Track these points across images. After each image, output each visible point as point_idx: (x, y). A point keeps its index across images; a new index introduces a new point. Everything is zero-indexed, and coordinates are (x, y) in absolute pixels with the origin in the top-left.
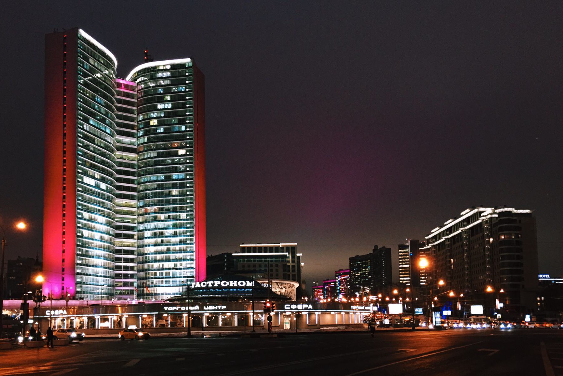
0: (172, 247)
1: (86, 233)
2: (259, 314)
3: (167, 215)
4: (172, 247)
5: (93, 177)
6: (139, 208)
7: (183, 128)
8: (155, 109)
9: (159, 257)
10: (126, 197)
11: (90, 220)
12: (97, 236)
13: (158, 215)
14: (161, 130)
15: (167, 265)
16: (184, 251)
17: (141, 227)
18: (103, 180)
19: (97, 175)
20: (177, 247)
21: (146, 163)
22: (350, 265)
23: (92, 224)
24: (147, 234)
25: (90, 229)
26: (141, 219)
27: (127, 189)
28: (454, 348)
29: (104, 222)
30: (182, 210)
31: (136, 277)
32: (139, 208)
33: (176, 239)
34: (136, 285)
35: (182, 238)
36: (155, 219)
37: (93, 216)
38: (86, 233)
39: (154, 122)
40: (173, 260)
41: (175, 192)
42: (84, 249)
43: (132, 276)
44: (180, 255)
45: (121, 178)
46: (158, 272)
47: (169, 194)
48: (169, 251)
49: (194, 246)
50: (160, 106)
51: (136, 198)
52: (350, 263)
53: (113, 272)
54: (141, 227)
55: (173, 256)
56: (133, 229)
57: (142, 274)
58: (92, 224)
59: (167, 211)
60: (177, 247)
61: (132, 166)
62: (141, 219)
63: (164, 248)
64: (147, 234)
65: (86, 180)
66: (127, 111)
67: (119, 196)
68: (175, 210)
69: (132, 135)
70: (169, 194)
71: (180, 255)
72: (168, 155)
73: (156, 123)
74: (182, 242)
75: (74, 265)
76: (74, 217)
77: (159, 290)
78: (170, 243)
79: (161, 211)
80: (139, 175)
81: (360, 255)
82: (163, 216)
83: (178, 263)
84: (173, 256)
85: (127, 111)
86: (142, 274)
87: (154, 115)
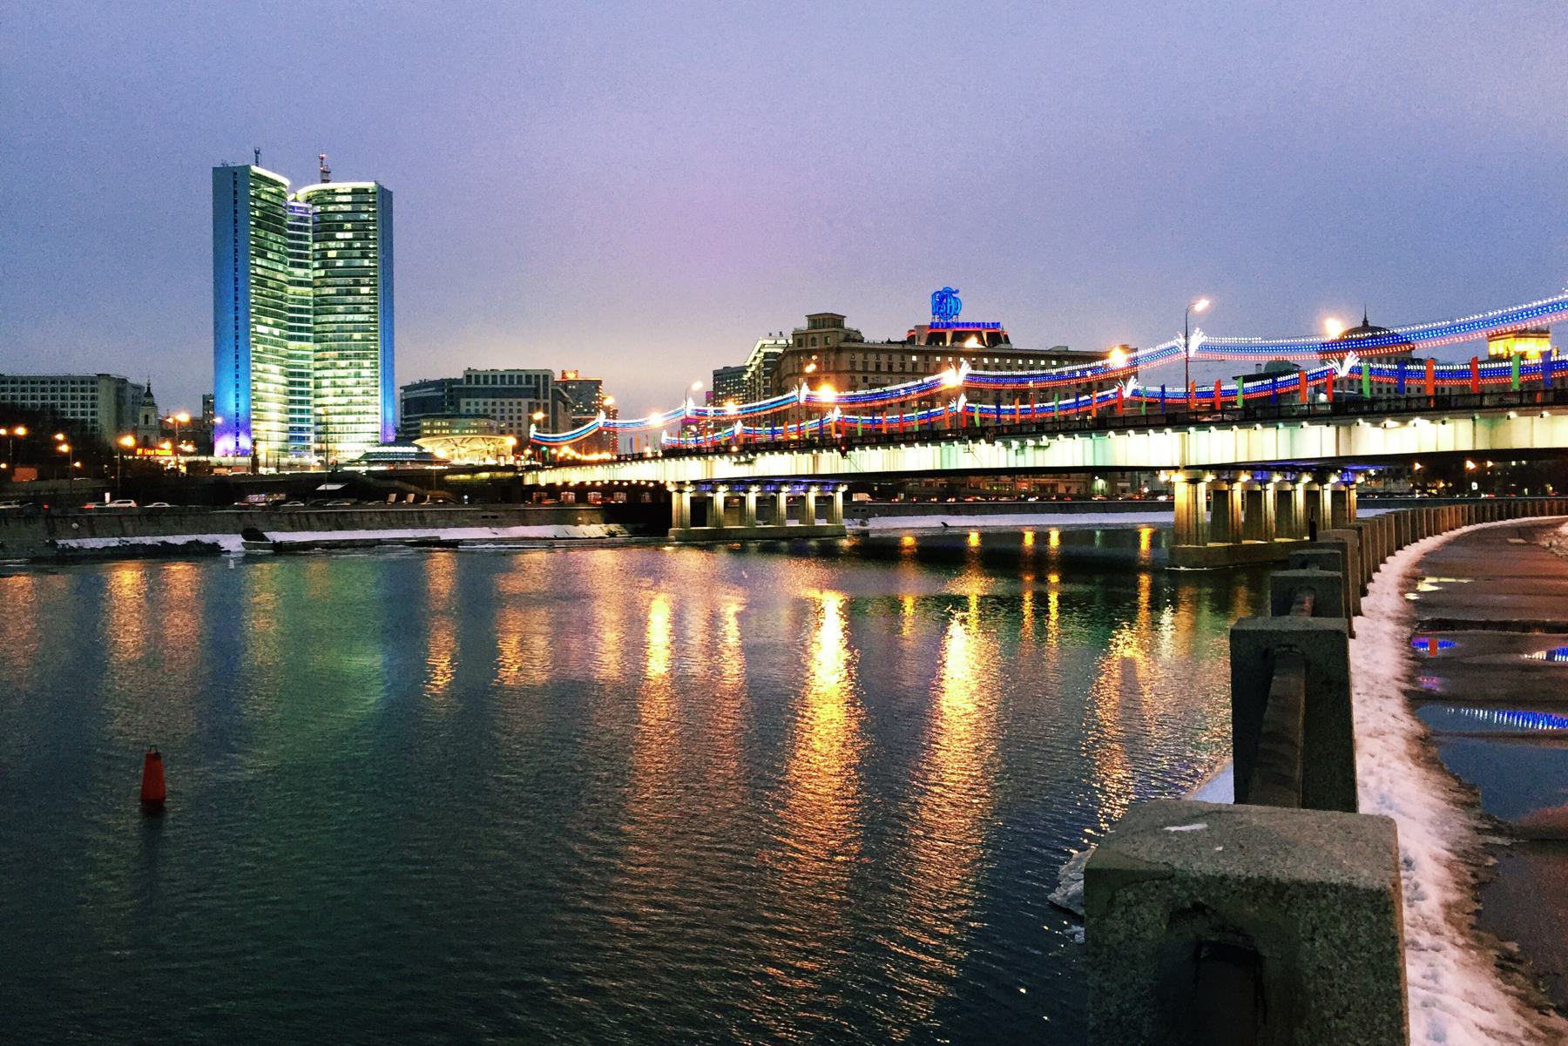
0: (354, 399)
1: (260, 386)
2: (962, 359)
3: (348, 362)
4: (354, 399)
5: (266, 324)
6: (315, 351)
7: (366, 262)
8: (335, 239)
9: (339, 409)
10: (301, 339)
11: (264, 371)
12: (271, 387)
13: (338, 362)
14: (340, 263)
15: (348, 418)
16: (366, 403)
17: (318, 374)
18: (276, 325)
19: (270, 321)
20: (360, 399)
21: (323, 300)
22: (714, 385)
23: (265, 376)
24: (325, 382)
25: (265, 381)
26: (318, 365)
27: (300, 329)
28: (1453, 580)
29: (278, 372)
30: (365, 357)
31: (312, 431)
32: (315, 351)
33: (358, 390)
34: (312, 421)
35: (366, 388)
36: (334, 366)
37: (267, 366)
38: (260, 386)
39: (332, 254)
40: (355, 413)
41: (357, 336)
42: (259, 403)
43: (308, 429)
44: (362, 408)
45: (293, 253)
46: (338, 426)
47: (350, 339)
48: (350, 403)
49: (379, 398)
50: (339, 235)
51: (312, 340)
52: (714, 381)
53: (287, 427)
54: (318, 374)
55: (355, 409)
56: (308, 375)
57: (320, 428)
58: (265, 376)
59: (347, 357)
60: (360, 399)
61: (307, 302)
62: (318, 365)
63: (344, 400)
64: (325, 382)
65: (260, 328)
66: (301, 320)
67: (292, 338)
68: (357, 356)
69: (306, 266)
70: (350, 339)
71: (362, 408)
72: (349, 293)
73: (335, 256)
74: (366, 393)
75: (249, 421)
76: (248, 372)
77: (338, 447)
78: (351, 394)
79: (342, 357)
80: (316, 314)
81: (732, 366)
82: (343, 363)
83: (361, 416)
84: (355, 409)
85: (301, 320)
86: (320, 428)
87: (332, 244)
